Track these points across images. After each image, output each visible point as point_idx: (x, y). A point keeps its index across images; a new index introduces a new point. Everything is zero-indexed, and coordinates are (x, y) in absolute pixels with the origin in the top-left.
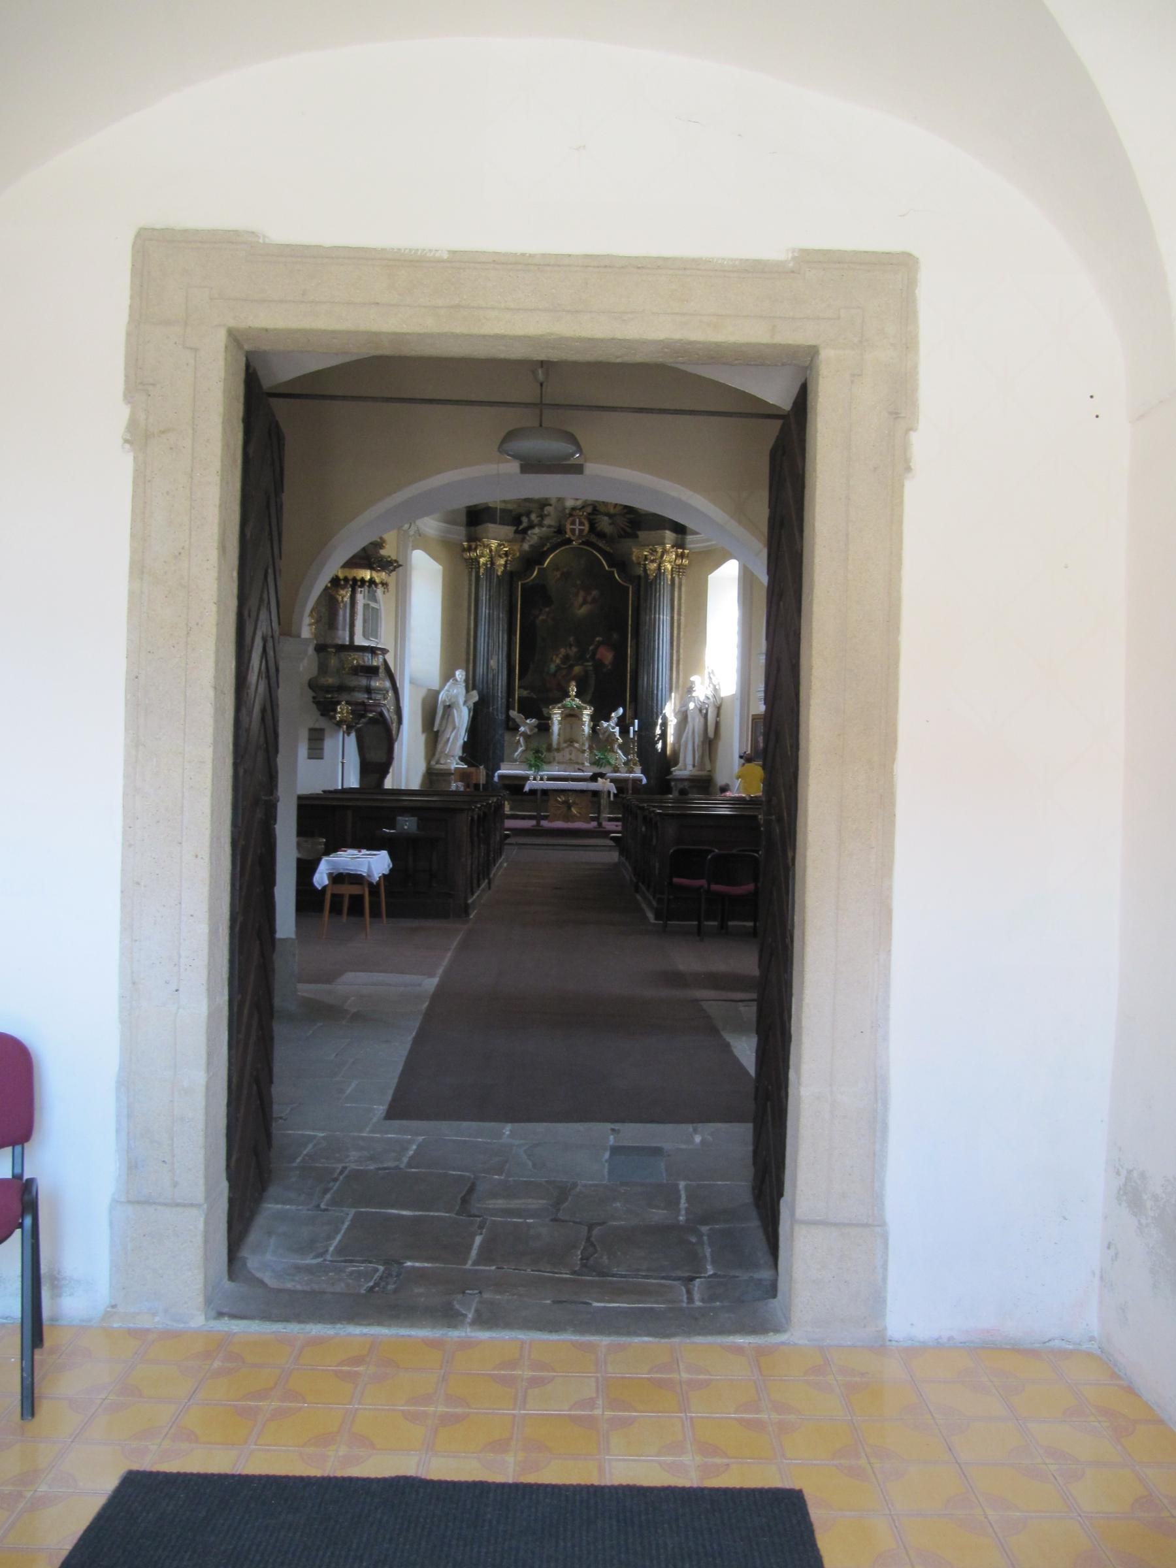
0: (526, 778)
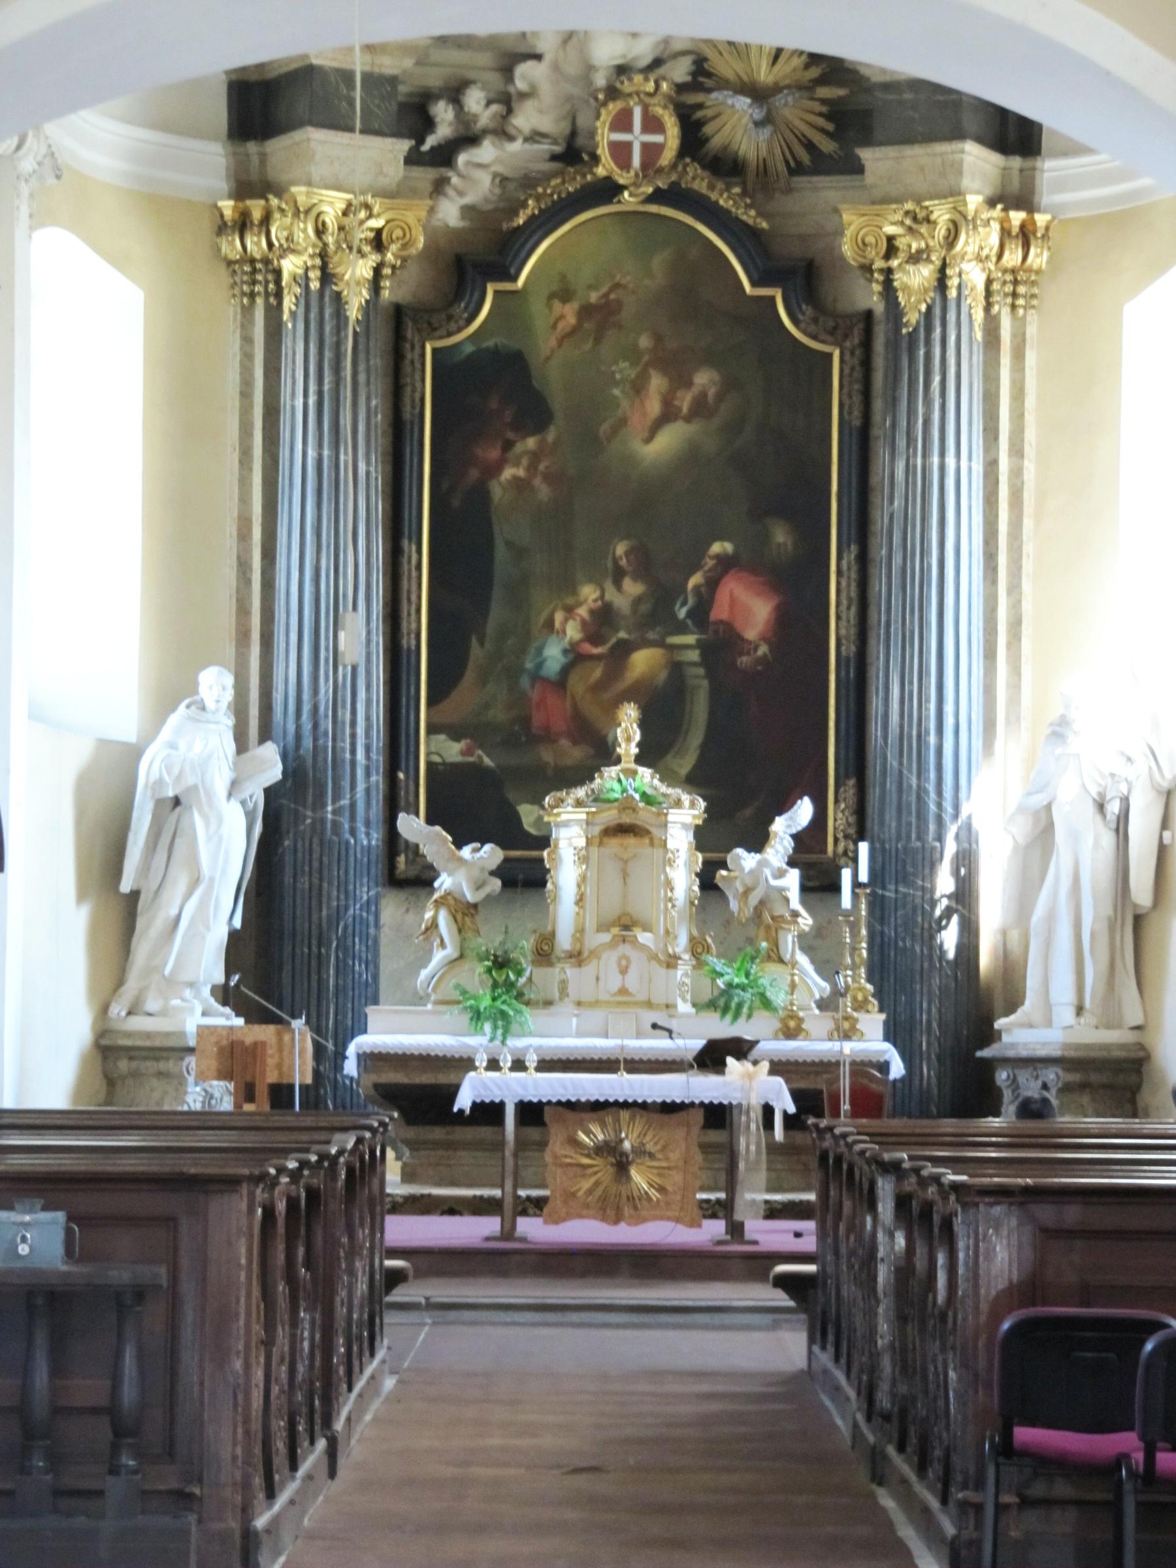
0: (465, 1064)
